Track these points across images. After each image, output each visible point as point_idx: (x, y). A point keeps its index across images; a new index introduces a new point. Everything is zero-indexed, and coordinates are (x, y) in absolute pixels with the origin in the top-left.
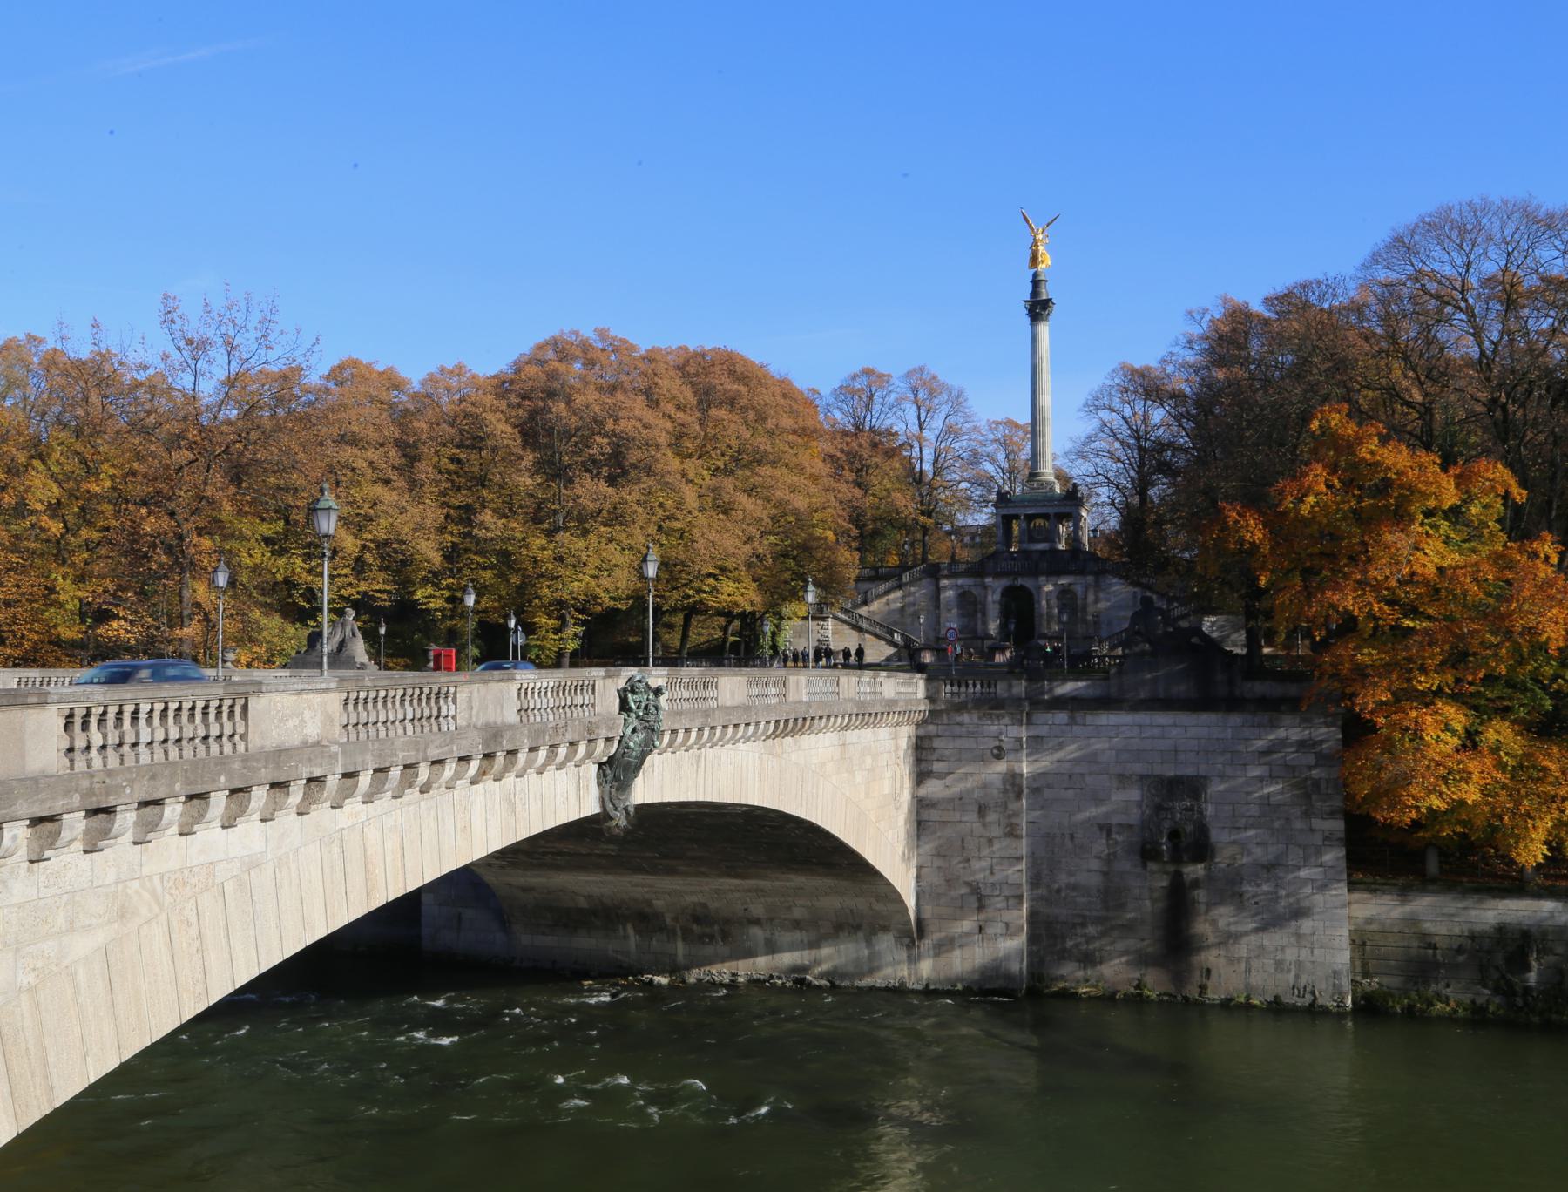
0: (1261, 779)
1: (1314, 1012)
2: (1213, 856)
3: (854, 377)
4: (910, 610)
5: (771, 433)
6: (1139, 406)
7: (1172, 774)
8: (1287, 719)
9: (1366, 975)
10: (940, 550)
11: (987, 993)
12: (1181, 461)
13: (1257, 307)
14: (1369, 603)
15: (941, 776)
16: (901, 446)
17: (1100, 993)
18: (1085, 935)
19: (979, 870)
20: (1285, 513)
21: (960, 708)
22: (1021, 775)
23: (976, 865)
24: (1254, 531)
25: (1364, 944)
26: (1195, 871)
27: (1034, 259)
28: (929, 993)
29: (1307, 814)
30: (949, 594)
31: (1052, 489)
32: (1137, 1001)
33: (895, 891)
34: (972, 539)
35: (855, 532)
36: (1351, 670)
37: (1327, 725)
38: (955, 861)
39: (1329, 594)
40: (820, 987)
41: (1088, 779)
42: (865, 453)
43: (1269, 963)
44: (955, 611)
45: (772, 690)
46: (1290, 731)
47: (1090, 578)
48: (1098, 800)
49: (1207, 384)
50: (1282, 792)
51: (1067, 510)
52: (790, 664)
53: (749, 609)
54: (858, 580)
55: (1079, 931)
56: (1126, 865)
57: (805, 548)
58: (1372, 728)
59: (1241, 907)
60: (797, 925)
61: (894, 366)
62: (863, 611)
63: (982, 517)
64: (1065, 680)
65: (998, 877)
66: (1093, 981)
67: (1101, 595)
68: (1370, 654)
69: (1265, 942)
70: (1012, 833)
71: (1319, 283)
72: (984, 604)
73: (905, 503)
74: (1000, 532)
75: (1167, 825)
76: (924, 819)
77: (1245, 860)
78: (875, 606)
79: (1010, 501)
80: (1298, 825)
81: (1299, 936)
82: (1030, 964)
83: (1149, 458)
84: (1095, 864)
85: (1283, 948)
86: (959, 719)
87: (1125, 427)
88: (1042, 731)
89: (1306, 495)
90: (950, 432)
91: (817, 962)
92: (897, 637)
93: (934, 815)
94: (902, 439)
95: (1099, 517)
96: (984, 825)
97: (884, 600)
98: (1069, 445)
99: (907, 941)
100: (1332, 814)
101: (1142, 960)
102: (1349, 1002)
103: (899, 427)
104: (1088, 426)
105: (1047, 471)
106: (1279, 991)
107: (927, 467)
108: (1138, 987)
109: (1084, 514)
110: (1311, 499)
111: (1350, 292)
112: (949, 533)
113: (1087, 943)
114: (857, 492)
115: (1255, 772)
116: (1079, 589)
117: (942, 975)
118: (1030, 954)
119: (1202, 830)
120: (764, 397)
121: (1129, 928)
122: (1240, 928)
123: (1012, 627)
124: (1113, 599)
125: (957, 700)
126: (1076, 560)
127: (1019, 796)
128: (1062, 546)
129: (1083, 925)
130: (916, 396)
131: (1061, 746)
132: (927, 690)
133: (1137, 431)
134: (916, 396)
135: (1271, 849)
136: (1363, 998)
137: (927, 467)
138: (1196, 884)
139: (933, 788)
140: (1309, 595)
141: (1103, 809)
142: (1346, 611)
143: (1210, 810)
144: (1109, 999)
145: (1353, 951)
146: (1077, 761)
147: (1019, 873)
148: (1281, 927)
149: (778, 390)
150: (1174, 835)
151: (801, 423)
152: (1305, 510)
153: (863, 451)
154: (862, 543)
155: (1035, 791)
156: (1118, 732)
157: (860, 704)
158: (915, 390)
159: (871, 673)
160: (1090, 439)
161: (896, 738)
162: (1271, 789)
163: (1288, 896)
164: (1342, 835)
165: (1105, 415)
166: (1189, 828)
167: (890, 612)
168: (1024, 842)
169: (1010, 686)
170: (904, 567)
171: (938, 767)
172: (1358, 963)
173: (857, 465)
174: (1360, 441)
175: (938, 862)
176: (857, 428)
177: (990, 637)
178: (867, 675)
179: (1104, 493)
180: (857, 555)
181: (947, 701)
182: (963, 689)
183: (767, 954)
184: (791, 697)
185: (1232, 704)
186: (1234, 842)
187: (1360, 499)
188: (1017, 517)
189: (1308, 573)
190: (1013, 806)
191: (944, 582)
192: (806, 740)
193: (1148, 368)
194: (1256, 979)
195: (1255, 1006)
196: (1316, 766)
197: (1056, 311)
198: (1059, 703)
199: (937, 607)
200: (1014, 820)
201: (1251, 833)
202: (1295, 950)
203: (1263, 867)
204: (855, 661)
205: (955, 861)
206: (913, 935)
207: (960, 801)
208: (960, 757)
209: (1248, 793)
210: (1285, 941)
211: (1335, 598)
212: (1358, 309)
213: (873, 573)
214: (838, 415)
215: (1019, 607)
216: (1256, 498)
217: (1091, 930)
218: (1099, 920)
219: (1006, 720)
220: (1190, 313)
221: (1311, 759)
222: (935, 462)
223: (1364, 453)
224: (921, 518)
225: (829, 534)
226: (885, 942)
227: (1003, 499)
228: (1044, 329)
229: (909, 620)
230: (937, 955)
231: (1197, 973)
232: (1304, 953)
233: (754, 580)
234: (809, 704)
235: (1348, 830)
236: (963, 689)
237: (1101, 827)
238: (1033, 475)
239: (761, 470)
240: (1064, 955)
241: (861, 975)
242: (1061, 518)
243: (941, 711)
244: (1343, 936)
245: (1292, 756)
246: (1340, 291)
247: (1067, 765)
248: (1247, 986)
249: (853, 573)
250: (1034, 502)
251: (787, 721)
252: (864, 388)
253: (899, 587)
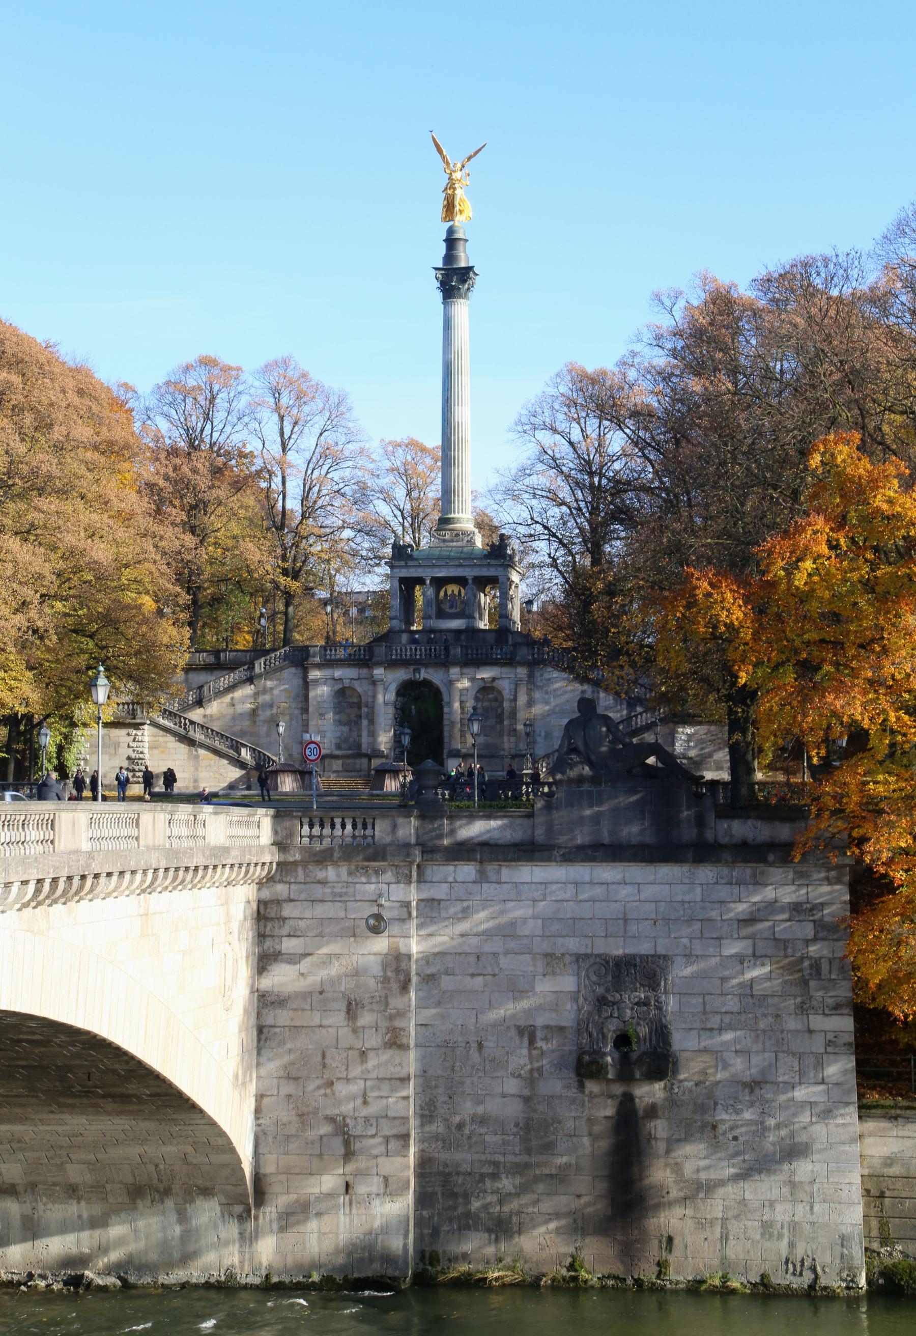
0: (741, 959)
1: (815, 1296)
2: (675, 1072)
3: (187, 369)
4: (264, 715)
5: (58, 448)
6: (592, 425)
7: (620, 952)
8: (777, 873)
9: (885, 1240)
10: (311, 630)
11: (356, 1281)
12: (645, 505)
13: (745, 291)
14: (884, 711)
15: (294, 959)
16: (258, 473)
17: (518, 1278)
18: (497, 1191)
19: (346, 1098)
20: (773, 585)
21: (322, 858)
22: (409, 956)
23: (342, 1089)
24: (732, 609)
25: (882, 1196)
26: (649, 1092)
27: (450, 208)
28: (270, 1288)
29: (803, 1009)
30: (321, 692)
31: (471, 542)
32: (571, 1287)
33: (222, 1134)
34: (361, 611)
35: (185, 598)
36: (860, 804)
37: (829, 881)
38: (311, 1086)
39: (830, 698)
40: (104, 1289)
41: (504, 961)
42: (202, 482)
43: (753, 1226)
44: (330, 716)
45: (33, 834)
46: (780, 889)
47: (522, 671)
48: (516, 990)
49: (680, 397)
50: (769, 978)
51: (492, 572)
52: (87, 793)
53: (22, 710)
54: (189, 669)
55: (489, 1184)
56: (557, 1085)
57: (109, 620)
58: (890, 887)
59: (716, 1146)
60: (73, 1191)
61: (247, 354)
62: (196, 715)
63: (373, 581)
64: (472, 817)
65: (373, 1108)
66: (508, 1260)
67: (537, 695)
68: (886, 783)
69: (748, 1196)
70: (395, 1042)
71: (826, 261)
72: (372, 707)
73: (259, 556)
74: (396, 602)
75: (612, 1028)
76: (268, 1024)
77: (719, 1076)
78: (215, 708)
79: (411, 557)
80: (792, 1023)
81: (793, 1185)
82: (419, 1238)
83: (604, 502)
84: (512, 1086)
85: (772, 1203)
86: (321, 875)
87: (572, 455)
88: (440, 891)
89: (800, 559)
90: (327, 455)
91: (103, 1249)
92: (245, 754)
93: (283, 1017)
94: (258, 464)
95: (534, 585)
96: (355, 1031)
97: (227, 699)
98: (494, 480)
99: (239, 1209)
100: (836, 1008)
101: (579, 1226)
102: (862, 1282)
103: (254, 445)
104: (521, 453)
105: (465, 518)
106: (767, 1267)
107: (293, 504)
108: (571, 1267)
109: (515, 577)
110: (808, 565)
111: (871, 277)
112: (325, 603)
113: (501, 1203)
114: (189, 540)
115: (733, 948)
116: (505, 686)
117: (290, 1261)
118: (420, 1222)
119: (661, 1033)
120: (46, 393)
121: (559, 1178)
122: (713, 1175)
123: (406, 740)
124: (549, 701)
125: (317, 846)
126: (503, 645)
127: (405, 987)
128: (483, 624)
129: (495, 1176)
130: (277, 401)
131: (466, 913)
132: (276, 832)
133: (589, 463)
134: (277, 401)
135: (755, 1060)
136: (882, 1274)
137: (293, 504)
138: (652, 1111)
139: (282, 977)
140: (806, 699)
141: (524, 1004)
142: (854, 723)
143: (671, 1004)
144: (530, 1286)
145: (867, 1205)
146: (488, 934)
147: (405, 1103)
148: (769, 1171)
149: (70, 384)
150: (623, 1040)
151: (105, 434)
152: (800, 580)
153: (198, 481)
154: (195, 615)
155: (429, 979)
156: (546, 891)
157: (171, 853)
158: (276, 392)
159: (189, 808)
160: (525, 472)
161: (227, 903)
162: (756, 973)
163: (778, 1127)
164: (852, 1039)
165: (546, 437)
166: (643, 1030)
167: (236, 717)
168: (412, 1054)
169: (395, 827)
170: (259, 651)
171: (289, 945)
172: (874, 1223)
173: (190, 500)
174: (875, 484)
175: (288, 1088)
176: (191, 444)
177: (378, 754)
178: (184, 811)
179: (543, 548)
180: (187, 632)
181: (303, 849)
182: (327, 831)
183: (24, 1240)
184: (64, 843)
185: (703, 852)
186: (705, 1050)
187: (874, 567)
188: (420, 581)
189: (807, 668)
190: (396, 1002)
191: (315, 674)
192: (84, 909)
193: (604, 373)
194: (735, 1251)
195: (733, 1291)
196: (815, 940)
197: (480, 284)
198: (463, 851)
199: (305, 710)
200: (398, 1023)
201: (728, 1036)
202: (789, 1206)
203: (745, 1085)
204: (162, 789)
205: (311, 1086)
206: (248, 1200)
207: (319, 996)
208: (323, 930)
209: (723, 979)
210: (775, 1193)
211: (839, 703)
212: (879, 299)
213: (211, 659)
214: (163, 425)
215: (421, 713)
216: (738, 561)
217: (506, 1184)
218: (518, 1169)
219: (389, 876)
220: (658, 297)
221: (809, 930)
222: (305, 498)
223: (879, 502)
224: (282, 580)
225: (148, 602)
226: (206, 1212)
227: (401, 553)
228: (462, 309)
229: (263, 729)
230: (283, 1229)
231: (655, 1243)
232: (801, 1210)
233: (30, 668)
234: (90, 855)
235: (860, 1031)
236: (327, 831)
237: (521, 1031)
238: (444, 522)
239: (43, 503)
240: (467, 1223)
241: (169, 1265)
242: (482, 583)
243: (295, 864)
244: (852, 1183)
245: (783, 926)
246: (854, 273)
247: (475, 941)
248: (724, 1260)
249: (183, 659)
250: (444, 560)
251: (55, 880)
252: (203, 386)
253: (250, 680)
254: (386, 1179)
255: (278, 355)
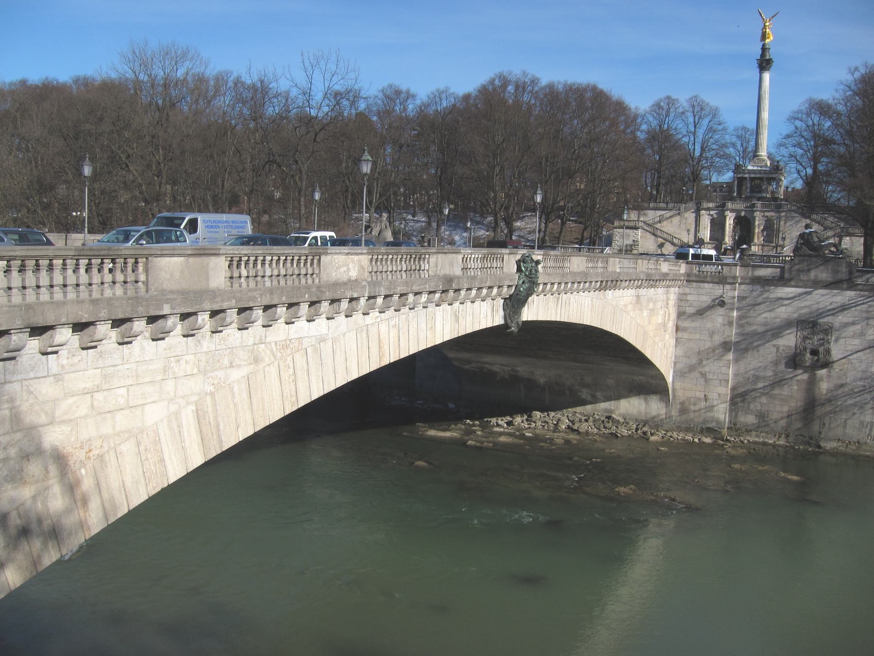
27: (764, 36)
90: (710, 130)
95: (792, 180)
157: (648, 275)
158: (693, 106)
165: (798, 123)
228: (767, 76)
234: (619, 273)
254: (719, 395)
255: (694, 94)
